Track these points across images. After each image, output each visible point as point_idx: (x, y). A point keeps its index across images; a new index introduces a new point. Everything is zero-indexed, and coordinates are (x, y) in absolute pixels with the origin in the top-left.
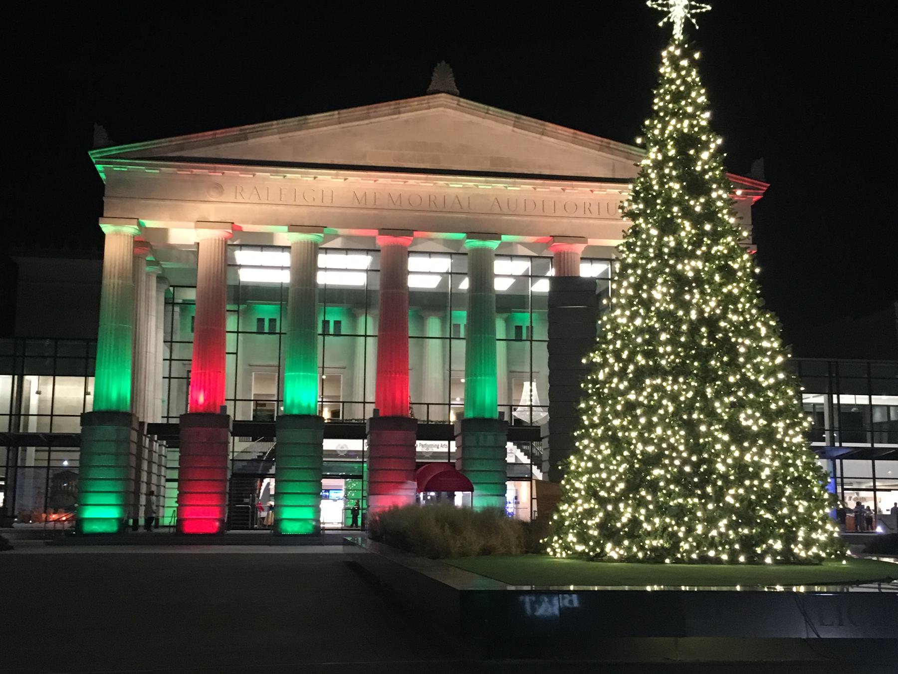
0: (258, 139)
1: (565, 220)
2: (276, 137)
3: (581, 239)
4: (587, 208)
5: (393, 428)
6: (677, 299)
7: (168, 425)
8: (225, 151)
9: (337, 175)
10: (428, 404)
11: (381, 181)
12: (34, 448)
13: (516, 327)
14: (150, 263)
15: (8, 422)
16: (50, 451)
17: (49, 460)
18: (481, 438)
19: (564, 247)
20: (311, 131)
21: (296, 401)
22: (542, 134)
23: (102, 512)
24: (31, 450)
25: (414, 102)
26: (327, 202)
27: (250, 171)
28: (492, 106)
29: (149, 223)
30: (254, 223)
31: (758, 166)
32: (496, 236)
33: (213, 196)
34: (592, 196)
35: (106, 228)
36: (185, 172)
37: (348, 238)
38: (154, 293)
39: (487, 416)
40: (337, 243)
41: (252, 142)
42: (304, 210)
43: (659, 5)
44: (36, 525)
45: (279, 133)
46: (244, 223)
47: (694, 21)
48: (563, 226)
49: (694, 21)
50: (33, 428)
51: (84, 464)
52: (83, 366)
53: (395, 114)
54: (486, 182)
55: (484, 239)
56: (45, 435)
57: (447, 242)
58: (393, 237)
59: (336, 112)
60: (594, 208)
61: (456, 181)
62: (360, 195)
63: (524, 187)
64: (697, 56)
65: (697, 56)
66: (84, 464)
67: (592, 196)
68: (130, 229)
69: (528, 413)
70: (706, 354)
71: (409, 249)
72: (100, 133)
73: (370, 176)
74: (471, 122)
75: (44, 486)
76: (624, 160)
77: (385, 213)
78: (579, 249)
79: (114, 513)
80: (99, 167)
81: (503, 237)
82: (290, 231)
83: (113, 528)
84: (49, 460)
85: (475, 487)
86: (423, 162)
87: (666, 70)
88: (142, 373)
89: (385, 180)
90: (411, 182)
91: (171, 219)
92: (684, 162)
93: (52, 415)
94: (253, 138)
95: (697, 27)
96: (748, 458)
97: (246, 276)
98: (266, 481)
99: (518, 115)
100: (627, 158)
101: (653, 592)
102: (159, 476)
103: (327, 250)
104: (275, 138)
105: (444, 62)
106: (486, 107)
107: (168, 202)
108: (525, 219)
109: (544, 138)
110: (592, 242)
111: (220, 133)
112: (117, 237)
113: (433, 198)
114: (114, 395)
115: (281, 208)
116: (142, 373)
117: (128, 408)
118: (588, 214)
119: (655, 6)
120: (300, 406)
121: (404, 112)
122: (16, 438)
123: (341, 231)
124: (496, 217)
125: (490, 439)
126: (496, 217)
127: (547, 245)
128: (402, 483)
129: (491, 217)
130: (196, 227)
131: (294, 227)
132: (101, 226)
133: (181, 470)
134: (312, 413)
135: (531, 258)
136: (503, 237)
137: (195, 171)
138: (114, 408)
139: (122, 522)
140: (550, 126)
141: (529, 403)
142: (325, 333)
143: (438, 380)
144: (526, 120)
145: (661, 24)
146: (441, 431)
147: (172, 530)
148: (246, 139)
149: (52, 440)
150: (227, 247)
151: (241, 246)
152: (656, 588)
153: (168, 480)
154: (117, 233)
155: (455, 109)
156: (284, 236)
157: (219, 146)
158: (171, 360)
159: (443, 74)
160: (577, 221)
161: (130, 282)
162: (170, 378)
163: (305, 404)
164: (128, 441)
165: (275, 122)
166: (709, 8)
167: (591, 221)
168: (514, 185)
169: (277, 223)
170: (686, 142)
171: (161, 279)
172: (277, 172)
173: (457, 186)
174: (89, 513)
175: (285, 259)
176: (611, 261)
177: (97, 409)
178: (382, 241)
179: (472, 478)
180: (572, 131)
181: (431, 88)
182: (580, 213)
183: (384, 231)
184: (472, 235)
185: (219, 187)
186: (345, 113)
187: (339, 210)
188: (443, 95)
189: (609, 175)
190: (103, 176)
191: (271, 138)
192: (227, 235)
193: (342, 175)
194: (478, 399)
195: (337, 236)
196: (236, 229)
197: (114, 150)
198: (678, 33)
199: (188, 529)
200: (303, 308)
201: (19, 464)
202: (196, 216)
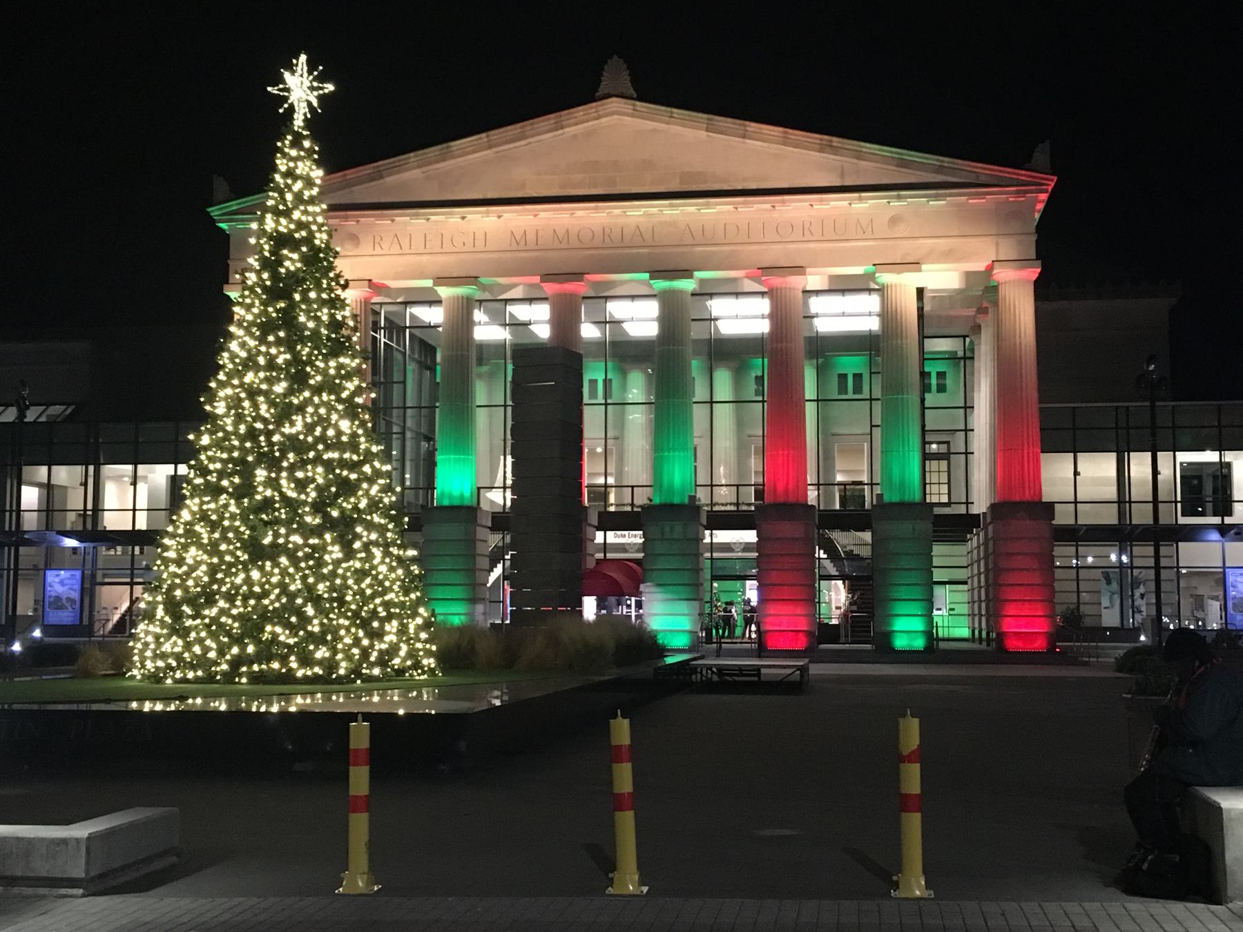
9: (488, 213)
10: (633, 487)
11: (542, 215)
13: (840, 376)
15: (1112, 472)
18: (667, 529)
20: (460, 160)
22: (744, 137)
25: (579, 112)
26: (480, 245)
27: (386, 216)
31: (1041, 155)
32: (686, 273)
39: (676, 500)
45: (419, 167)
48: (774, 254)
53: (557, 130)
54: (671, 206)
58: (572, 278)
59: (484, 135)
61: (633, 207)
72: (221, 186)
73: (528, 210)
74: (654, 131)
76: (855, 161)
77: (550, 254)
86: (595, 186)
89: (548, 216)
93: (1076, 502)
96: (242, 576)
99: (710, 116)
101: (152, 712)
105: (615, 57)
106: (669, 109)
108: (725, 248)
113: (607, 231)
115: (425, 258)
118: (808, 237)
120: (450, 496)
121: (569, 126)
124: (685, 249)
126: (685, 249)
134: (467, 503)
140: (753, 126)
148: (382, 177)
152: (159, 707)
155: (632, 116)
157: (354, 189)
159: (616, 72)
160: (793, 246)
163: (456, 493)
165: (412, 155)
167: (812, 245)
168: (708, 206)
172: (417, 215)
178: (550, 288)
180: (781, 129)
181: (603, 89)
183: (548, 277)
184: (656, 274)
186: (495, 134)
187: (492, 255)
188: (614, 99)
189: (837, 182)
193: (493, 212)
194: (666, 478)
197: (234, 205)
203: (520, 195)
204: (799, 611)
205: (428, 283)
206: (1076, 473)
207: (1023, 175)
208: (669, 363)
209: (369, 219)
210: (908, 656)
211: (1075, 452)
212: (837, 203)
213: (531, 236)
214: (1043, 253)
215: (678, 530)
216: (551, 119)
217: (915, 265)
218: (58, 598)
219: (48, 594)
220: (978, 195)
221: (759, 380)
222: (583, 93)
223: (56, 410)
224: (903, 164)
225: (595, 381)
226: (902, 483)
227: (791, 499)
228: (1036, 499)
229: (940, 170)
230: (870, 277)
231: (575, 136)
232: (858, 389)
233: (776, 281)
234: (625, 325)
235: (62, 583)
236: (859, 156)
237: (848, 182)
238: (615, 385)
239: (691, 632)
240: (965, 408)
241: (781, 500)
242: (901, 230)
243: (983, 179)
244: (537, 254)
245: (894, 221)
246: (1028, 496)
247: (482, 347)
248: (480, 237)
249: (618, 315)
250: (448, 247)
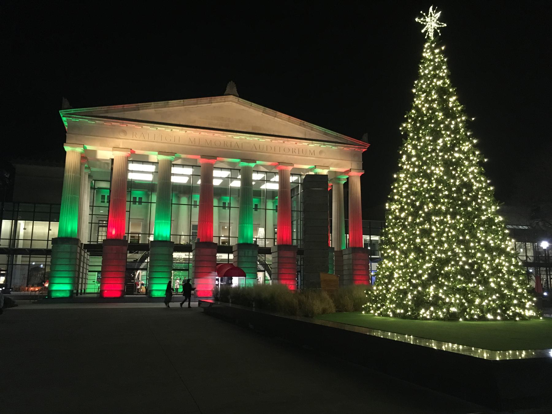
0: (147, 110)
1: (284, 156)
2: (153, 110)
3: (291, 164)
4: (293, 151)
5: (204, 246)
6: (447, 172)
7: (90, 245)
8: (127, 115)
11: (202, 133)
12: (21, 256)
14: (86, 168)
16: (30, 257)
17: (30, 261)
18: (247, 252)
19: (283, 167)
20: (171, 108)
21: (160, 234)
22: (275, 117)
23: (61, 287)
24: (20, 257)
25: (218, 98)
28: (254, 103)
29: (89, 147)
30: (142, 150)
31: (365, 137)
32: (254, 161)
33: (122, 136)
34: (296, 146)
35: (67, 148)
36: (108, 124)
37: (184, 159)
38: (87, 182)
39: (249, 242)
40: (179, 162)
43: (422, 21)
44: (22, 293)
45: (155, 108)
46: (137, 149)
47: (439, 31)
49: (439, 31)
50: (21, 246)
51: (53, 265)
52: (52, 215)
54: (250, 137)
55: (249, 162)
56: (28, 249)
57: (230, 163)
60: (297, 151)
63: (267, 140)
64: (443, 48)
65: (443, 48)
66: (53, 265)
67: (296, 146)
68: (80, 150)
69: (264, 242)
70: (460, 201)
71: (214, 166)
72: (66, 102)
74: (243, 110)
75: (27, 274)
76: (310, 130)
78: (290, 168)
79: (68, 287)
80: (64, 119)
81: (257, 162)
82: (159, 154)
83: (67, 295)
84: (30, 261)
85: (247, 274)
86: (222, 126)
87: (427, 54)
88: (79, 221)
90: (216, 135)
91: (101, 146)
92: (443, 102)
93: (32, 240)
94: (143, 109)
95: (432, 22)
97: (131, 176)
98: (138, 271)
100: (312, 130)
102: (86, 269)
103: (174, 165)
104: (152, 111)
107: (99, 138)
109: (276, 118)
110: (296, 166)
111: (126, 106)
112: (72, 153)
113: (226, 143)
114: (69, 230)
116: (79, 221)
117: (75, 236)
119: (420, 21)
120: (162, 237)
122: (12, 250)
123: (183, 156)
125: (250, 253)
127: (276, 166)
128: (210, 273)
129: (251, 153)
130: (113, 150)
131: (160, 153)
132: (65, 147)
133: (103, 267)
135: (266, 172)
136: (257, 162)
137: (113, 123)
138: (69, 236)
139: (71, 291)
140: (279, 114)
143: (225, 226)
144: (268, 110)
145: (432, 22)
146: (227, 249)
147: (96, 295)
148: (139, 110)
149: (31, 252)
150: (128, 161)
151: (133, 161)
153: (89, 271)
154: (73, 151)
155: (237, 103)
156: (154, 157)
157: (126, 112)
158: (92, 215)
160: (289, 156)
161: (78, 175)
162: (92, 223)
163: (164, 235)
164: (76, 252)
166: (445, 25)
167: (296, 157)
168: (263, 138)
169: (153, 150)
170: (442, 91)
171: (90, 176)
172: (153, 126)
173: (237, 138)
174: (55, 287)
175: (152, 168)
176: (301, 175)
177: (60, 236)
179: (245, 271)
181: (226, 93)
182: (291, 153)
183: (203, 157)
184: (243, 160)
185: (124, 132)
186: (186, 101)
190: (66, 124)
191: (151, 110)
192: (128, 155)
195: (180, 158)
196: (133, 152)
197: (72, 111)
198: (431, 35)
200: (165, 191)
201: (14, 263)
202: (113, 145)
203: (193, 125)
206: (49, 230)
207: (360, 142)
211: (50, 222)
212: (305, 143)
214: (365, 167)
224: (326, 134)
229: (336, 137)
231: (214, 107)
236: (312, 129)
237: (307, 137)
239: (121, 291)
240: (93, 206)
241: (285, 243)
242: (323, 155)
243: (349, 142)
244: (199, 147)
245: (321, 152)
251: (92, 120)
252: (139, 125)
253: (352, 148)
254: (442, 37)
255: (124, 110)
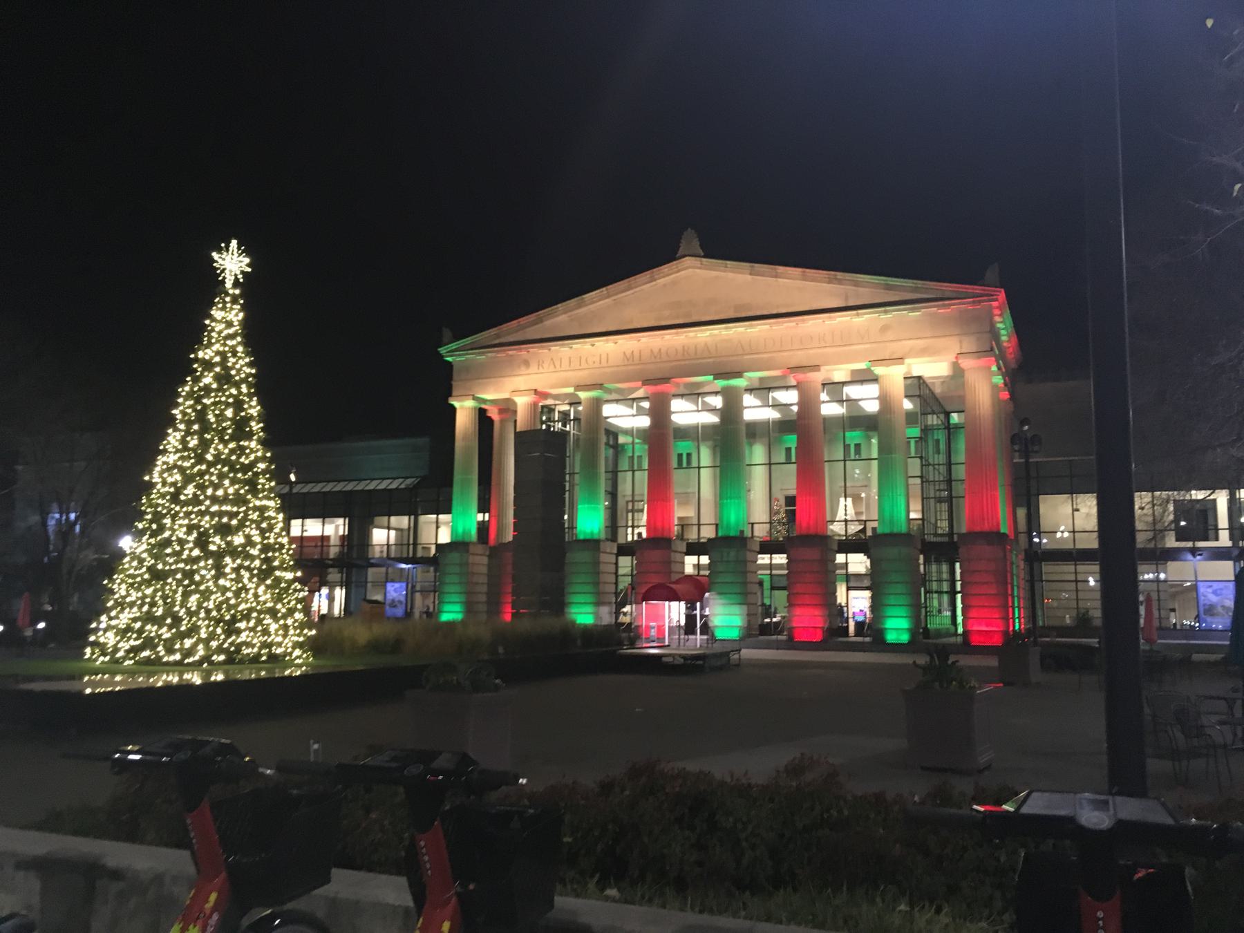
8: (531, 333)
11: (643, 340)
20: (591, 307)
25: (665, 268)
26: (604, 363)
31: (992, 274)
32: (738, 374)
33: (523, 370)
35: (456, 404)
36: (501, 354)
39: (732, 534)
41: (548, 323)
42: (586, 372)
45: (565, 313)
46: (552, 387)
55: (728, 378)
58: (659, 383)
62: (628, 353)
72: (447, 333)
95: (232, 263)
103: (608, 401)
134: (596, 537)
140: (781, 269)
141: (843, 518)
142: (680, 466)
145: (232, 263)
159: (690, 239)
163: (588, 530)
168: (751, 326)
178: (651, 389)
181: (680, 253)
183: (646, 382)
184: (718, 376)
185: (527, 363)
191: (561, 317)
194: (725, 519)
197: (453, 346)
199: (975, 641)
204: (817, 613)
205: (571, 390)
207: (977, 289)
208: (729, 437)
209: (534, 349)
210: (897, 648)
213: (636, 354)
215: (733, 554)
216: (645, 276)
217: (900, 360)
218: (393, 601)
219: (1201, 603)
220: (944, 306)
221: (788, 450)
222: (665, 254)
223: (409, 481)
224: (889, 288)
225: (938, 441)
226: (892, 522)
227: (812, 532)
228: (995, 530)
229: (915, 290)
230: (868, 371)
231: (665, 285)
232: (689, 462)
233: (801, 376)
234: (861, 403)
235: (395, 590)
236: (857, 284)
237: (851, 304)
238: (863, 448)
242: (890, 335)
243: (947, 295)
245: (885, 328)
246: (986, 527)
247: (827, 421)
248: (604, 357)
249: (854, 396)
250: (584, 365)
251: (479, 354)
252: (543, 348)
253: (955, 308)
254: (248, 284)
255: (523, 328)
